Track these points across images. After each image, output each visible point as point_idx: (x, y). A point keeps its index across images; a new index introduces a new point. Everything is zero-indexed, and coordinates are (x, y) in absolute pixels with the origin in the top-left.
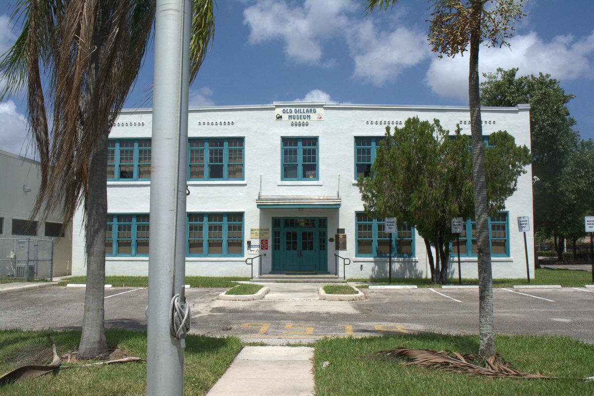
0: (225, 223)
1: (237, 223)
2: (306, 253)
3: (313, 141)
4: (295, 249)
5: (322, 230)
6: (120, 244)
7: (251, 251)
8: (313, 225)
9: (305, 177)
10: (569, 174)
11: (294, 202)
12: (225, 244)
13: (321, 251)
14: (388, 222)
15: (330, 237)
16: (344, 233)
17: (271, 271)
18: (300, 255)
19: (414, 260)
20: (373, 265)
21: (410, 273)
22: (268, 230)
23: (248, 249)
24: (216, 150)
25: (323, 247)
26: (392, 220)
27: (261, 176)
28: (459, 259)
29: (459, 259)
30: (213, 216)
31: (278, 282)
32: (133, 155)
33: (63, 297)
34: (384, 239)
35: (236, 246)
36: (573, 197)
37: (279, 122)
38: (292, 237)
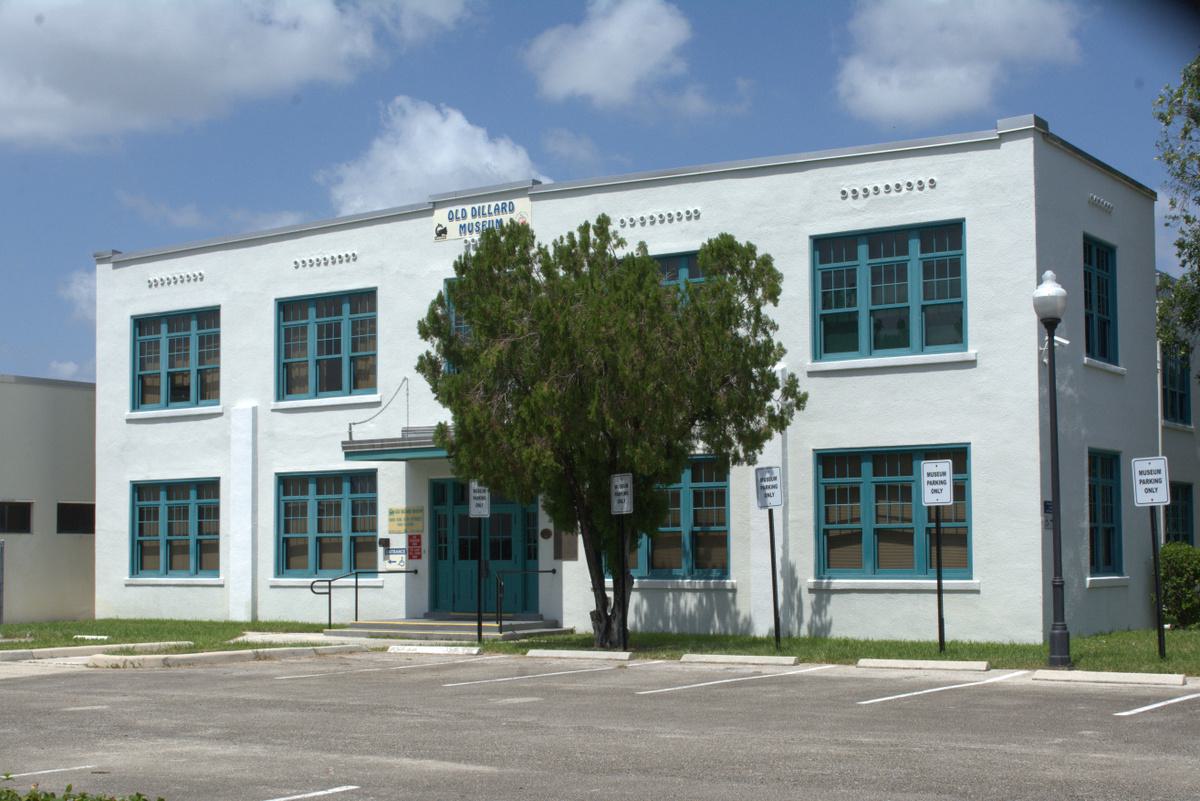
1: (152, 503)
2: (496, 566)
7: (390, 562)
15: (545, 527)
17: (427, 610)
18: (482, 573)
19: (824, 586)
21: (722, 619)
22: (422, 511)
23: (385, 559)
25: (532, 554)
28: (940, 585)
29: (940, 585)
32: (306, 339)
33: (335, 671)
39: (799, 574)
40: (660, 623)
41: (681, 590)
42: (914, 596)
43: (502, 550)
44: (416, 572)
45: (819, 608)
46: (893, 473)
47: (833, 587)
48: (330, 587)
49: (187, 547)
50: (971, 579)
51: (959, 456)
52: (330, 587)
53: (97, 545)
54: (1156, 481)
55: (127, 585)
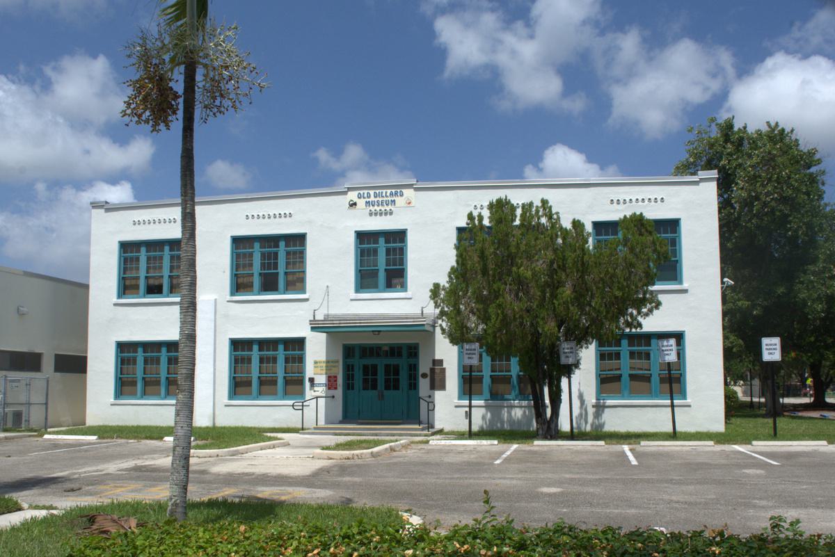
0: (281, 353)
1: (297, 352)
2: (389, 394)
3: (400, 236)
4: (374, 387)
5: (412, 361)
6: (146, 383)
8: (400, 355)
9: (389, 286)
10: (814, 273)
11: (360, 323)
12: (280, 382)
13: (348, 391)
14: (767, 345)
16: (442, 365)
17: (341, 419)
18: (381, 397)
19: (601, 404)
20: (483, 410)
22: (337, 362)
23: (310, 389)
24: (269, 253)
25: (414, 386)
26: (473, 347)
27: (328, 287)
28: (470, 403)
29: (470, 403)
30: (265, 344)
31: (336, 434)
33: (476, 458)
34: (500, 374)
35: (294, 385)
36: (819, 307)
37: (353, 211)
38: (370, 371)
39: (586, 397)
40: (499, 425)
41: (513, 407)
42: (654, 409)
43: (392, 384)
44: (333, 397)
45: (598, 415)
46: (243, 350)
47: (607, 404)
48: (303, 406)
49: (160, 381)
50: (686, 399)
51: (679, 337)
52: (303, 406)
53: (88, 380)
54: (774, 349)
55: (112, 405)
